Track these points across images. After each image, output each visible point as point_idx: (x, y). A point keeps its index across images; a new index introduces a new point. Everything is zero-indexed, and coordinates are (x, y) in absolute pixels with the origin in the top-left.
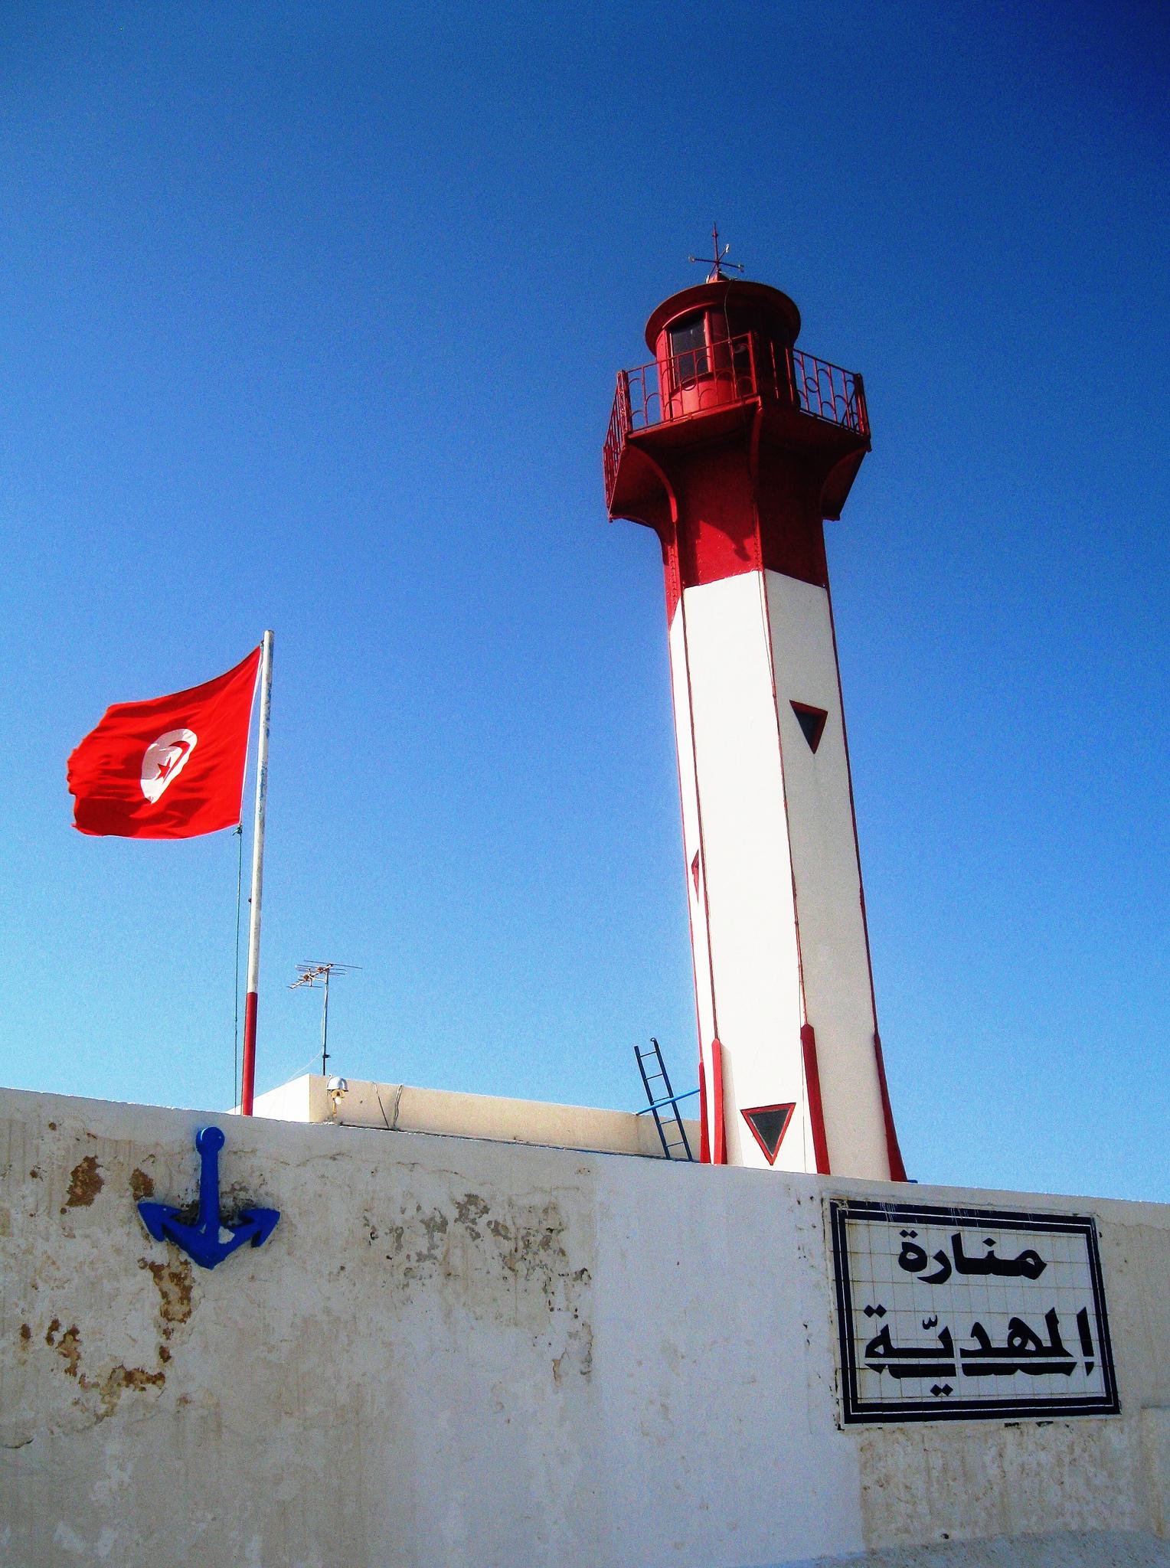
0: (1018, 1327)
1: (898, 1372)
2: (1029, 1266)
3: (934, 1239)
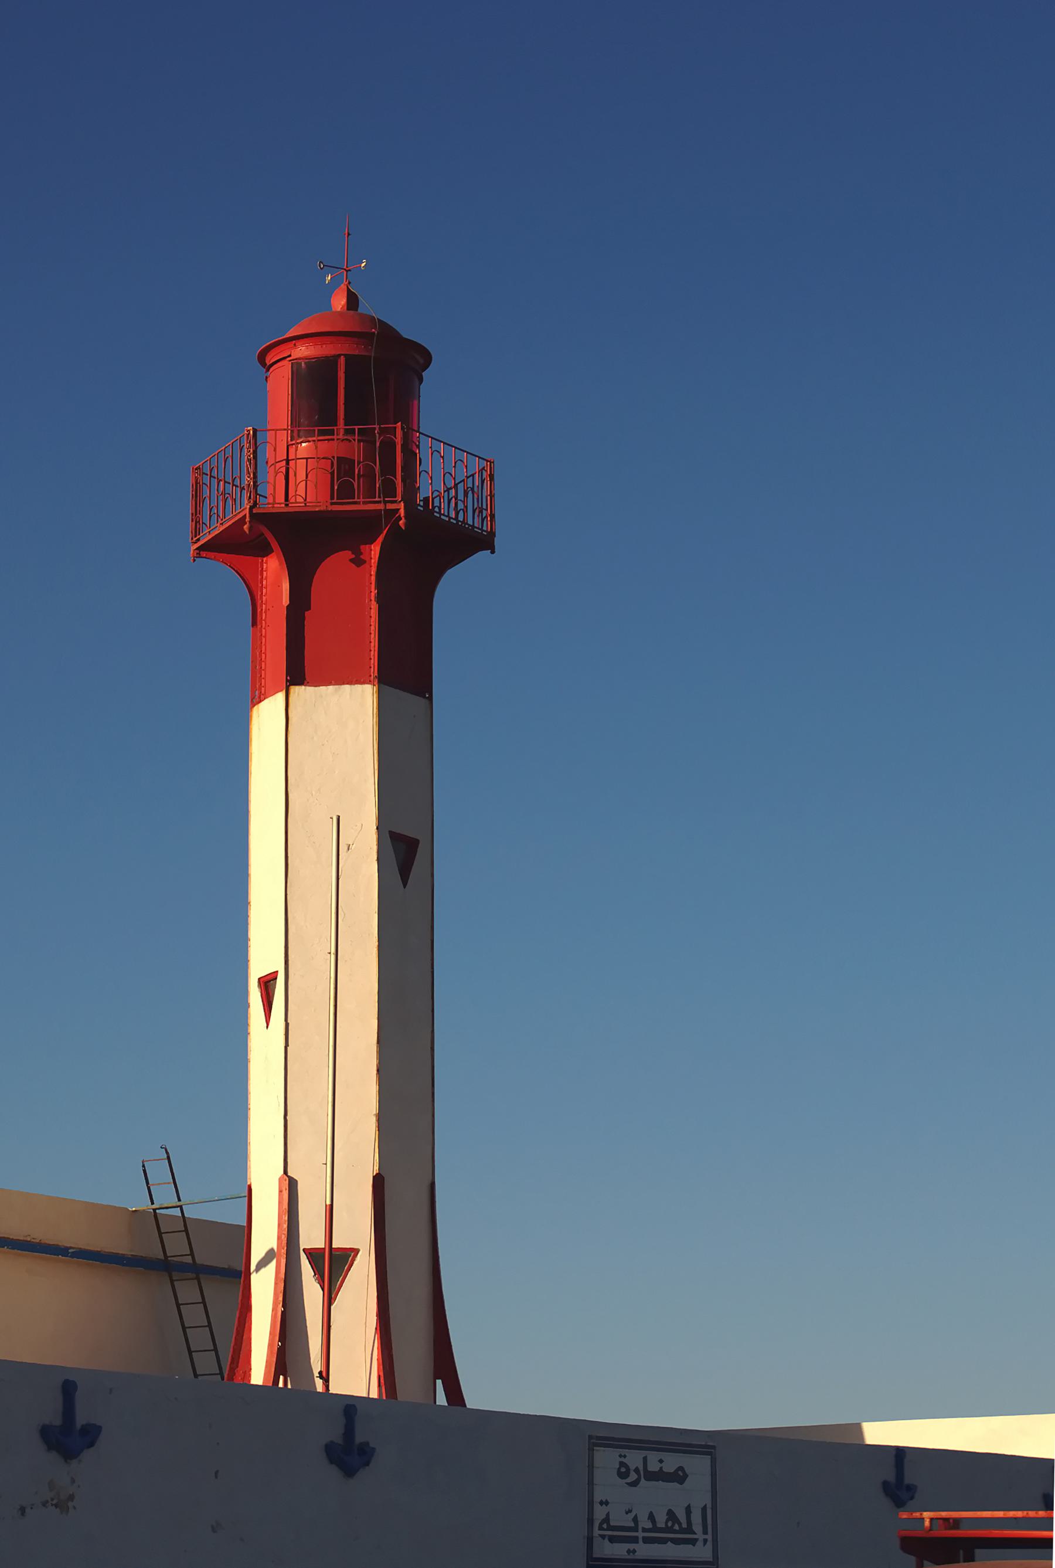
0: (671, 1515)
1: (612, 1540)
2: (679, 1477)
3: (634, 1459)
